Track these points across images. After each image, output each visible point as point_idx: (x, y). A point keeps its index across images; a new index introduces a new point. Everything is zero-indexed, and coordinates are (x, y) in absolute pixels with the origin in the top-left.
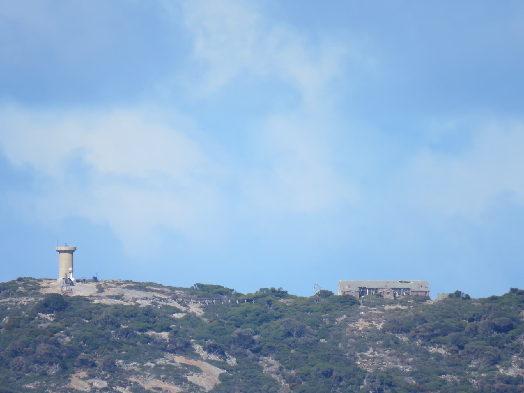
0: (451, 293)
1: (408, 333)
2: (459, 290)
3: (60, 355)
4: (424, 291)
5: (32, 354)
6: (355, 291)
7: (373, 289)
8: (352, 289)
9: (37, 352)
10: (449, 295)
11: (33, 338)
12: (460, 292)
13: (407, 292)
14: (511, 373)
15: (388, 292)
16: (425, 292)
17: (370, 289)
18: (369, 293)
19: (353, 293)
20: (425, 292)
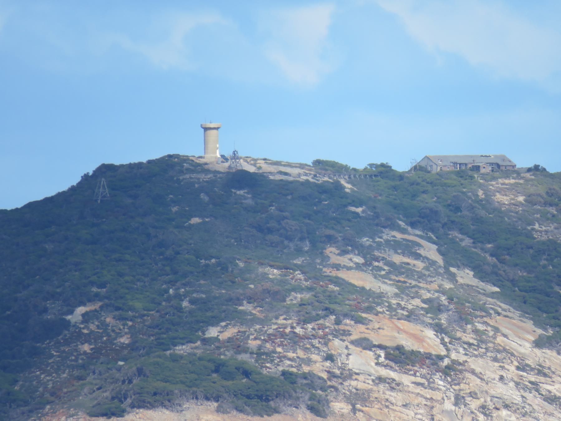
0: (530, 166)
1: (408, 226)
2: (537, 164)
3: (550, 346)
4: (511, 166)
5: (161, 381)
6: (443, 166)
7: (463, 164)
8: (445, 163)
9: (126, 378)
10: (527, 169)
11: (220, 332)
12: (539, 166)
13: (493, 166)
14: (218, 268)
15: (484, 166)
16: (512, 167)
17: (460, 164)
18: (459, 167)
19: (448, 167)
20: (512, 167)
